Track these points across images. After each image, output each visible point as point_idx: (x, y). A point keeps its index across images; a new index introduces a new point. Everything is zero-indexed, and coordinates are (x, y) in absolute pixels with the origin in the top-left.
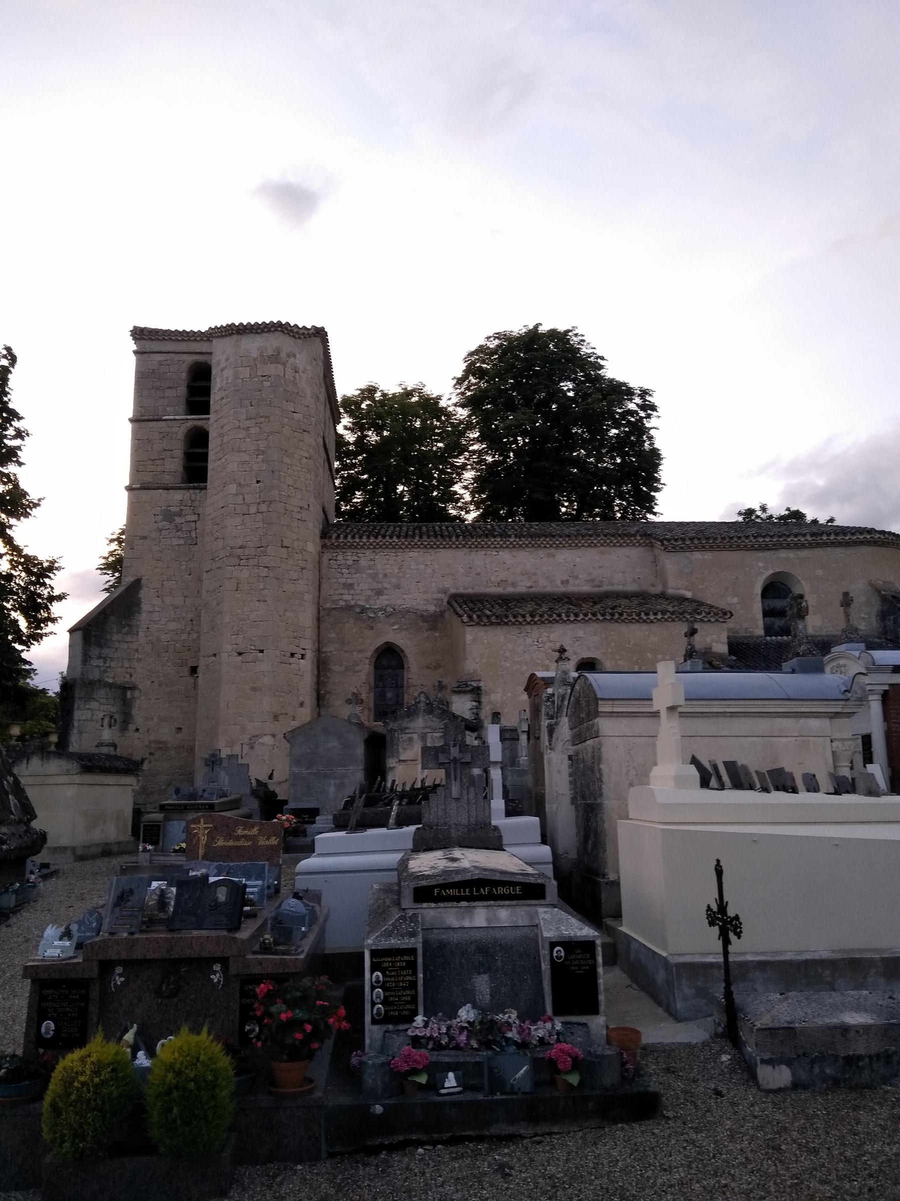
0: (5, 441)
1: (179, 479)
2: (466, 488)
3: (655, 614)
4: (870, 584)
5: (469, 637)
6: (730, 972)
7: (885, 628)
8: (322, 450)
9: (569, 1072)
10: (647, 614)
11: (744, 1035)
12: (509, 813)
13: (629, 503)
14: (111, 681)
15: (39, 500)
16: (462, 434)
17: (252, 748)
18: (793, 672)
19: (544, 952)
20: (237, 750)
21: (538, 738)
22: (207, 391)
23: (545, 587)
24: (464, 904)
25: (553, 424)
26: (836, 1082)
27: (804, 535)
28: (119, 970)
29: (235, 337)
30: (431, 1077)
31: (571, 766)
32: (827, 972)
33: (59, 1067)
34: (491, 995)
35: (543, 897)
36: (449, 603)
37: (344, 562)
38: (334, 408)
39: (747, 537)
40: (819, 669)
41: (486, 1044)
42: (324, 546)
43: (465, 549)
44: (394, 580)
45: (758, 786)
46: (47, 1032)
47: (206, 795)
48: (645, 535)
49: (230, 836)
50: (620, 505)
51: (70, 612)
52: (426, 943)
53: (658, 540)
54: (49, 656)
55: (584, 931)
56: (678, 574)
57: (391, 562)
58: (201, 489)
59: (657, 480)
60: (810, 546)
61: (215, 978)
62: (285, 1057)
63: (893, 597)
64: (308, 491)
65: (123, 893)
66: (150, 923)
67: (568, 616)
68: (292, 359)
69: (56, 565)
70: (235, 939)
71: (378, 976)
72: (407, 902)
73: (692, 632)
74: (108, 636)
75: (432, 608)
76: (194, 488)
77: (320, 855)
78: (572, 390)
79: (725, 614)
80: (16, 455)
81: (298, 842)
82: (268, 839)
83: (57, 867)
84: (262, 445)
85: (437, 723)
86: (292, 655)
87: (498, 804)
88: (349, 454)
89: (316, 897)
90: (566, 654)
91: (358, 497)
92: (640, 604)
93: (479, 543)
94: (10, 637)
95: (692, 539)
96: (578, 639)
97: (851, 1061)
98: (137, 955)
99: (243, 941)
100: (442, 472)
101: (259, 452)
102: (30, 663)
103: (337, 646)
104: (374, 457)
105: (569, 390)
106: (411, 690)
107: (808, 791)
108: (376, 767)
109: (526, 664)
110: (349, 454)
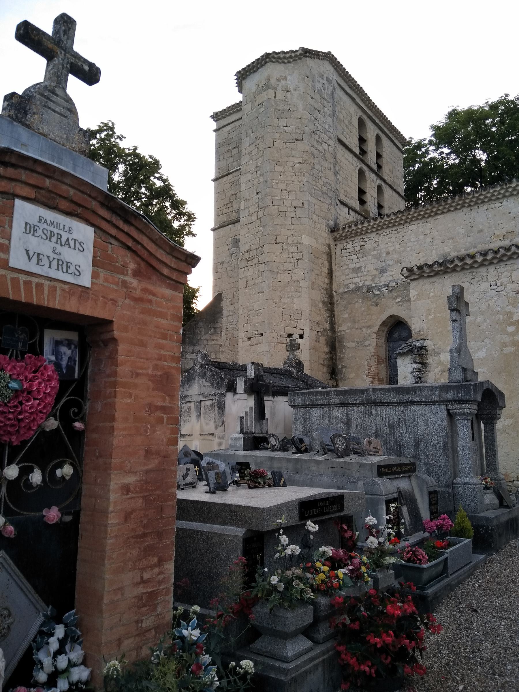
43: (465, 210)
44: (396, 256)
57: (393, 239)
68: (283, 82)
74: (199, 337)
93: (478, 199)
103: (349, 324)
109: (482, 313)
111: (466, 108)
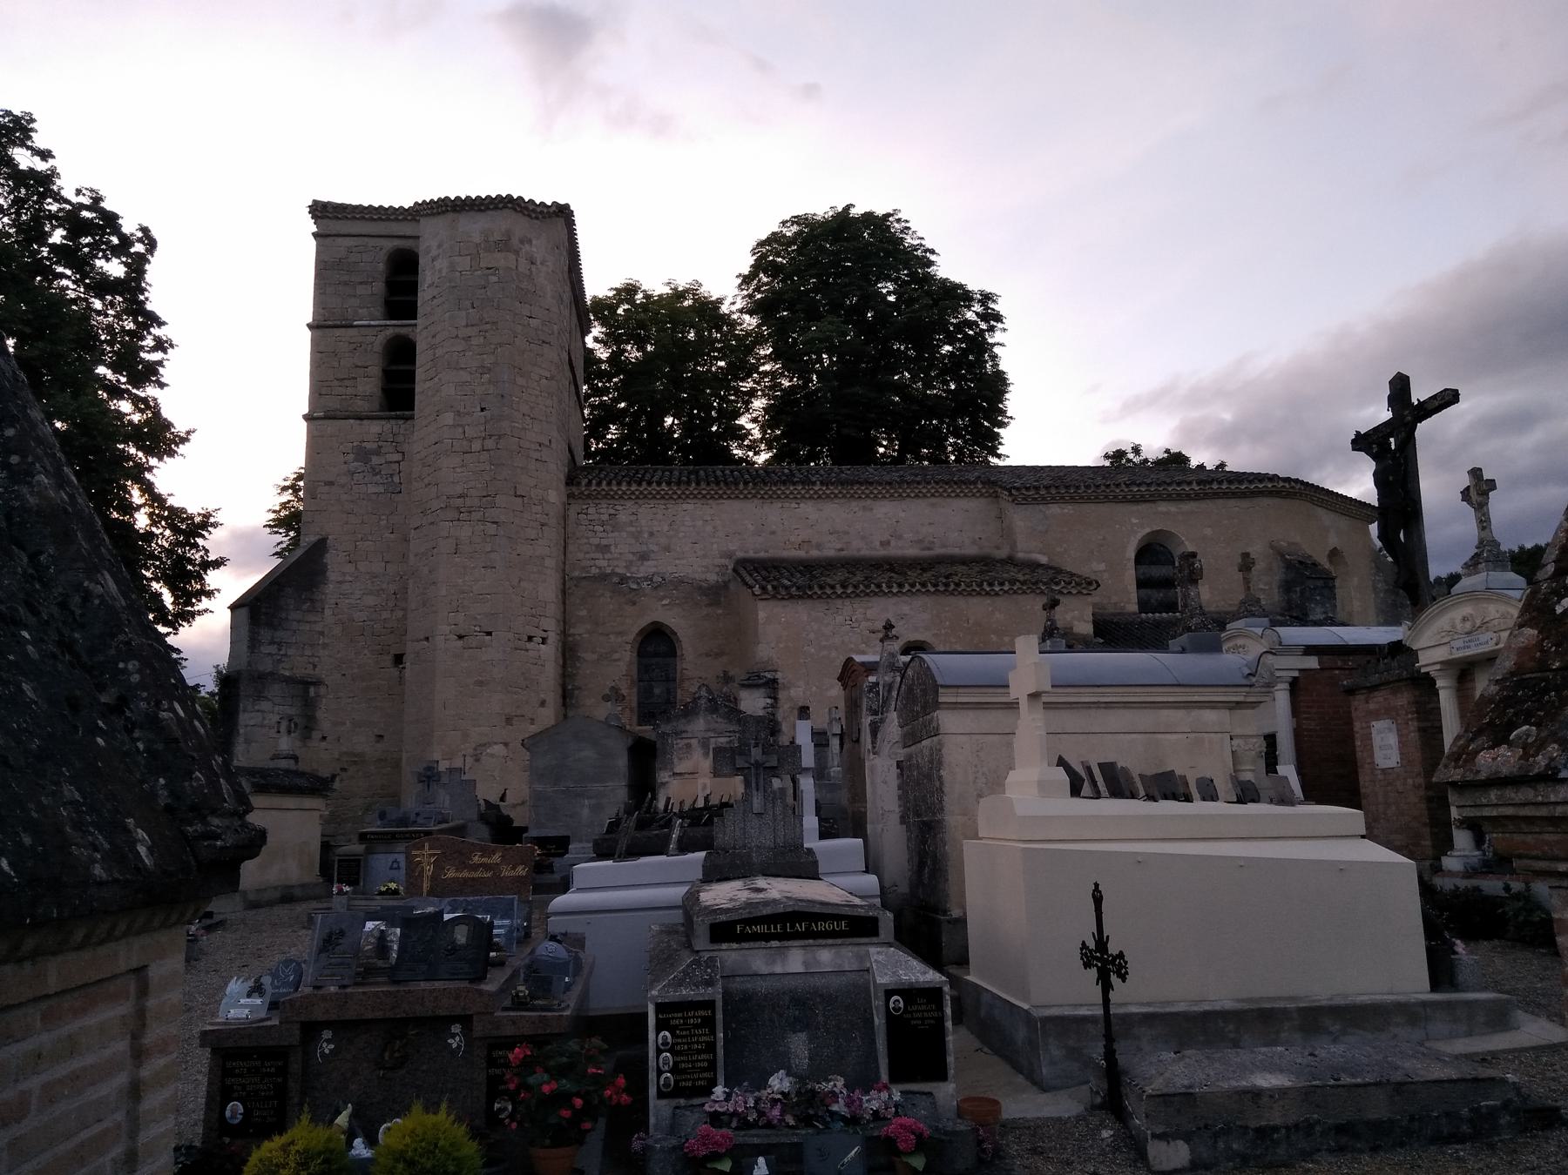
0: (143, 355)
1: (376, 406)
2: (754, 420)
3: (1002, 584)
4: (1272, 547)
5: (762, 615)
6: (1111, 1027)
7: (1289, 602)
8: (567, 368)
9: (911, 1154)
10: (990, 584)
11: (1130, 1104)
12: (823, 835)
13: (965, 442)
14: (287, 673)
15: (188, 433)
16: (750, 350)
17: (477, 760)
18: (1183, 651)
19: (878, 1003)
20: (458, 763)
21: (858, 741)
22: (413, 288)
24: (775, 943)
25: (869, 334)
26: (1245, 1160)
27: (1190, 483)
28: (327, 1034)
29: (451, 216)
30: (736, 1163)
31: (901, 775)
32: (1231, 1027)
33: (254, 1159)
34: (810, 1059)
35: (876, 933)
36: (734, 570)
37: (596, 517)
38: (583, 311)
39: (1118, 485)
40: (1215, 647)
41: (805, 1121)
42: (570, 496)
45: (1142, 793)
46: (232, 1117)
47: (420, 820)
48: (988, 483)
49: (463, 865)
50: (954, 445)
51: (229, 585)
52: (727, 995)
53: (1005, 489)
54: (204, 638)
55: (928, 976)
56: (1031, 533)
57: (660, 516)
58: (407, 419)
59: (1003, 412)
60: (1198, 497)
61: (454, 1043)
62: (548, 1142)
63: (1301, 563)
64: (547, 425)
65: (330, 935)
66: (367, 974)
67: (890, 587)
69: (212, 520)
70: (481, 993)
71: (665, 1038)
72: (701, 942)
73: (1053, 604)
75: (712, 578)
76: (397, 418)
77: (580, 890)
78: (894, 293)
79: (1090, 583)
80: (156, 373)
81: (548, 873)
82: (514, 868)
83: (221, 917)
84: (488, 360)
85: (722, 724)
86: (530, 638)
87: (811, 822)
88: (601, 375)
89: (578, 942)
90: (894, 632)
91: (613, 432)
92: (981, 572)
94: (151, 616)
95: (1047, 488)
97: (1263, 1133)
98: (351, 1014)
99: (490, 994)
100: (723, 399)
101: (484, 370)
102: (178, 651)
104: (634, 378)
105: (889, 293)
106: (686, 684)
107: (1204, 799)
108: (643, 783)
110: (601, 375)
111: (659, 289)
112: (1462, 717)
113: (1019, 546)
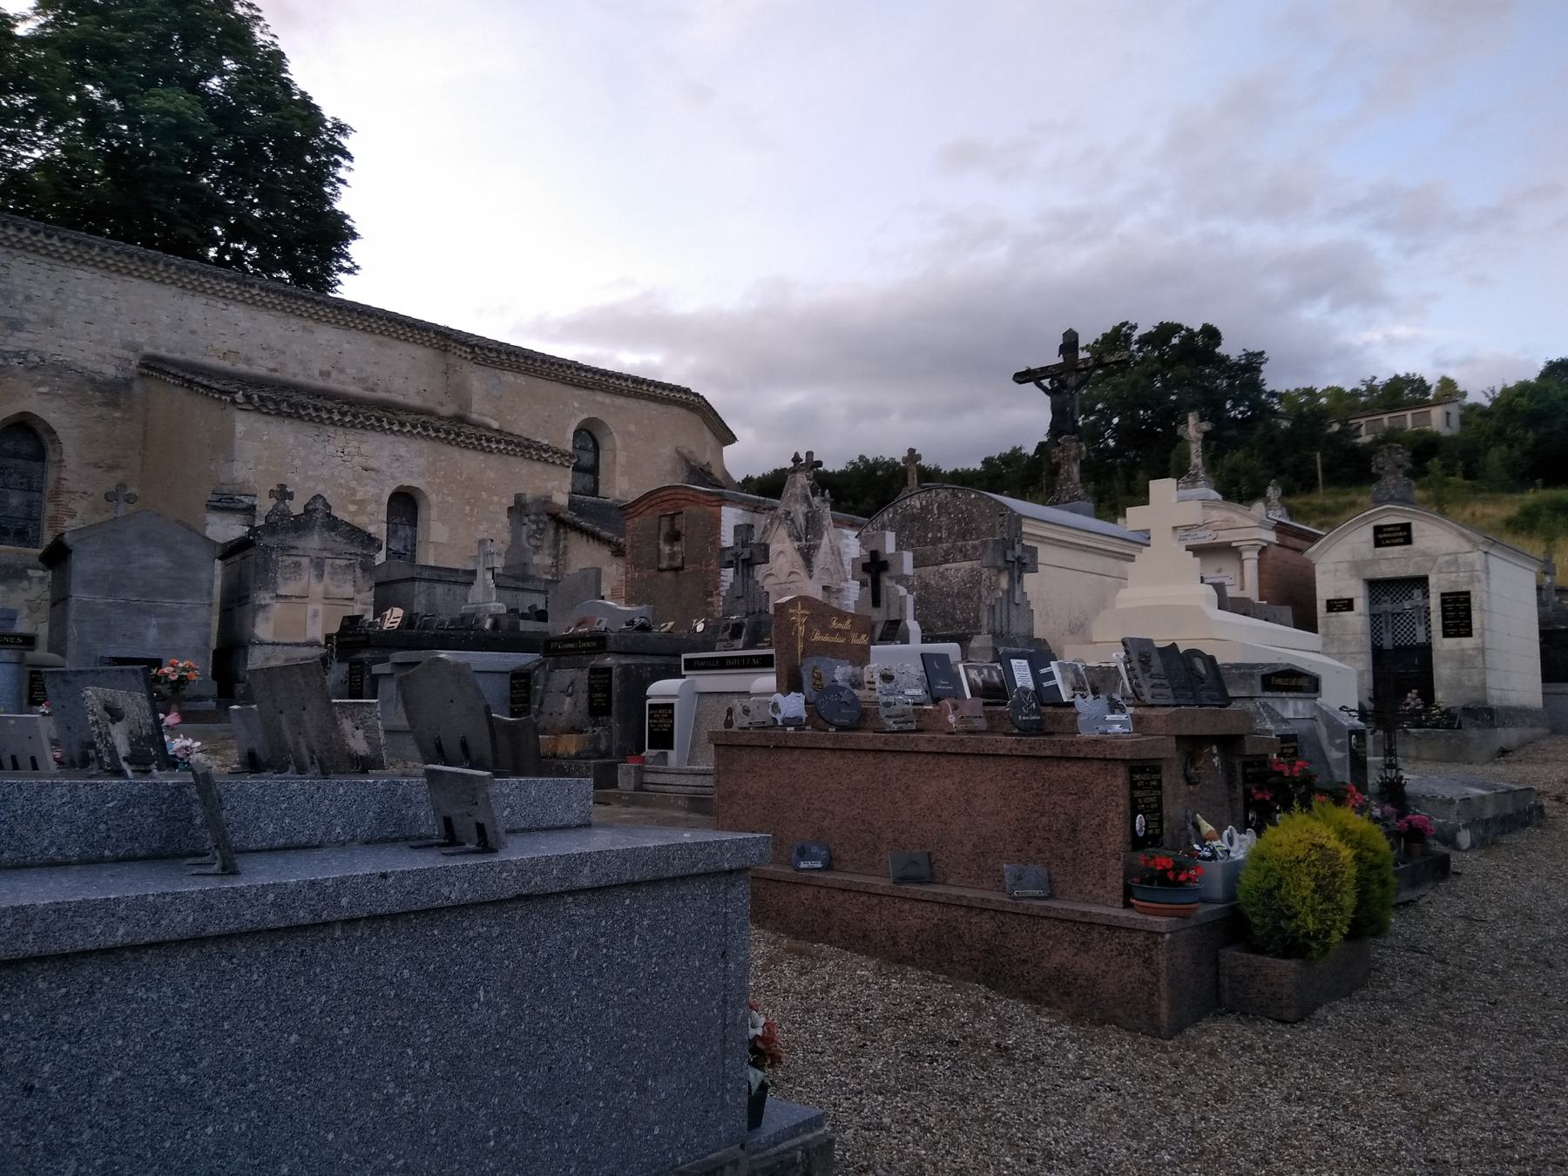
4: (678, 452)
5: (240, 428)
23: (295, 375)
43: (174, 288)
49: (825, 630)
75: (110, 371)
93: (201, 284)
96: (398, 458)
112: (1260, 580)
113: (475, 406)
